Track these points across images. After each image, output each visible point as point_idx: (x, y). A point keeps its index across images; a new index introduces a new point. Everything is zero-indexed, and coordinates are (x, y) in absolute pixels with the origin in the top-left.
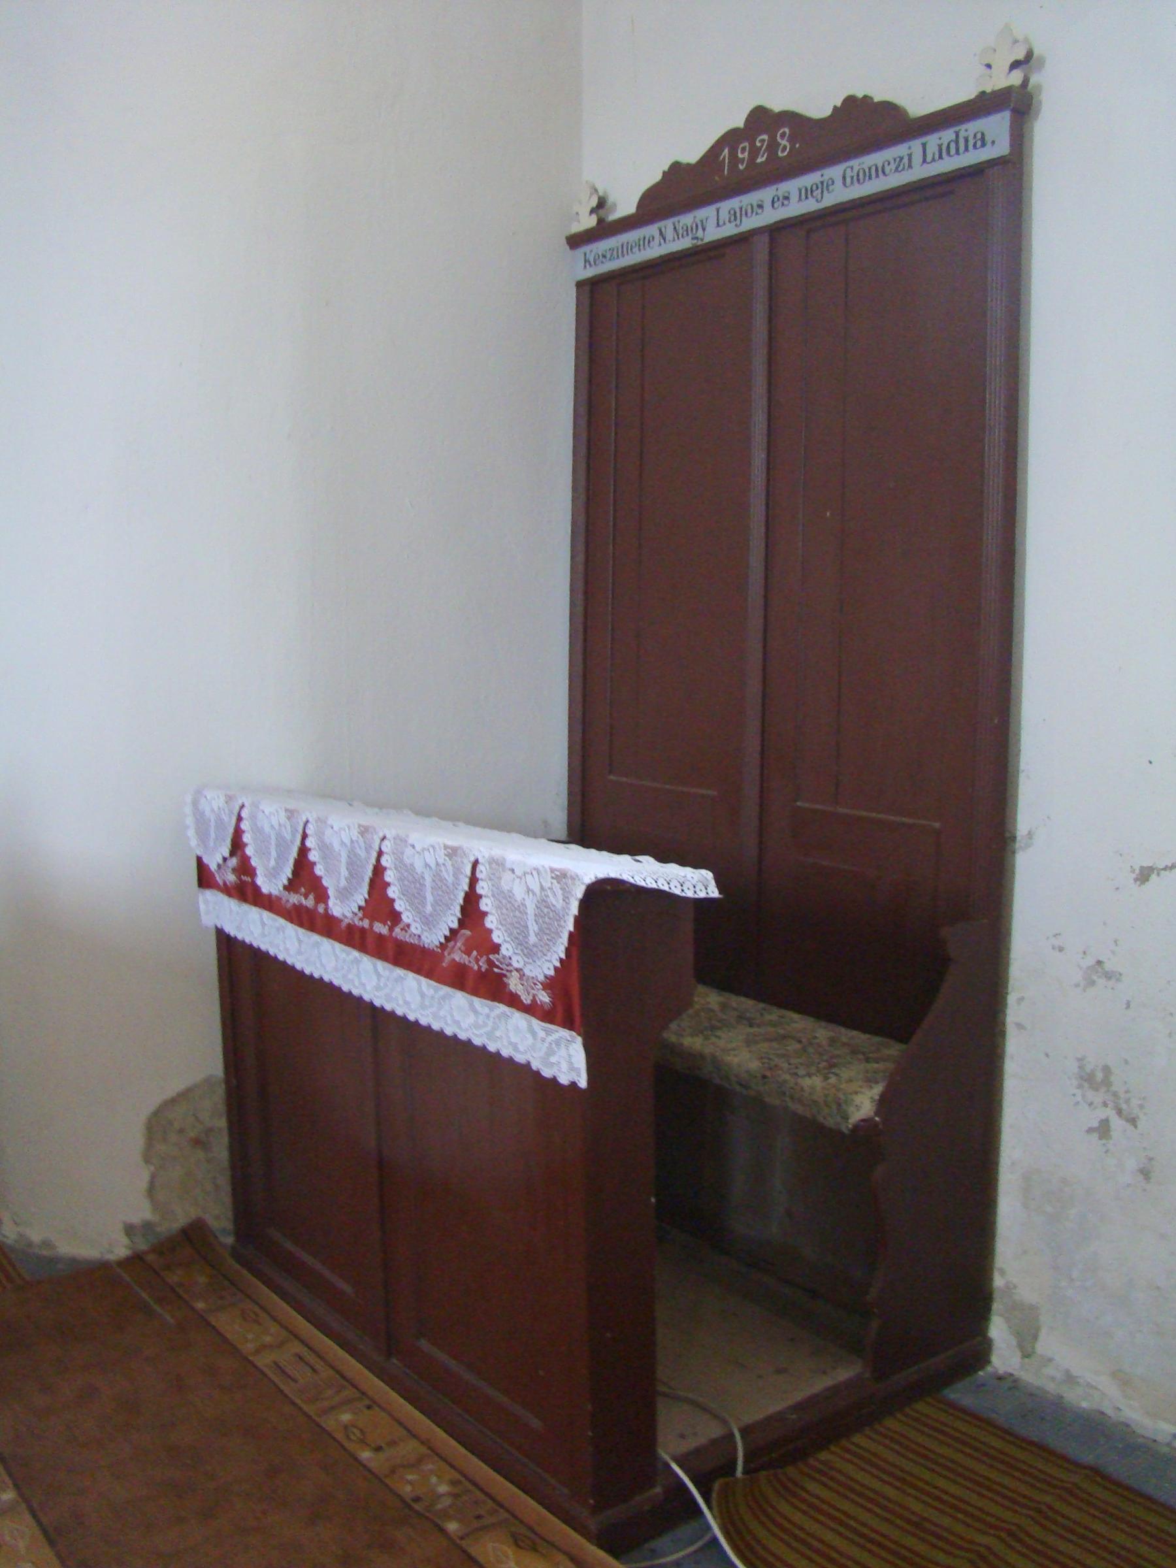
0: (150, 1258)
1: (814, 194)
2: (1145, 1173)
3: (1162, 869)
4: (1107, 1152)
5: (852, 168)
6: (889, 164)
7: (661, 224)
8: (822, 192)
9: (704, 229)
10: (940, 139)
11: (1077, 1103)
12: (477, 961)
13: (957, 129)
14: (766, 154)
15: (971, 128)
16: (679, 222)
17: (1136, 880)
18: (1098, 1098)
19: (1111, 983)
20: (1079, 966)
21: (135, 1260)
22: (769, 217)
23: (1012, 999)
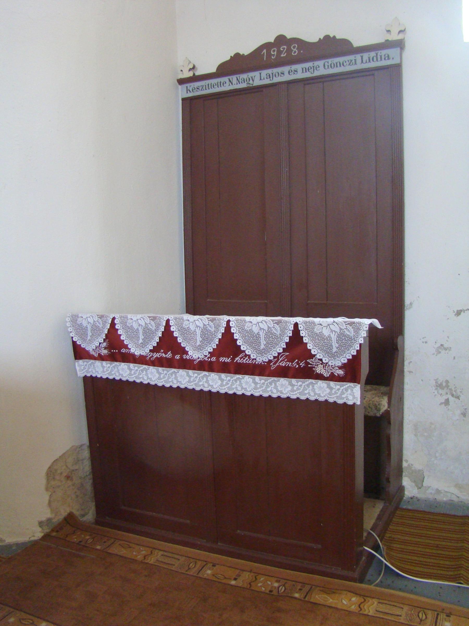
0: (54, 534)
1: (310, 70)
2: (464, 414)
3: (465, 310)
4: (448, 410)
5: (328, 62)
6: (346, 62)
7: (230, 77)
8: (314, 70)
9: (253, 81)
10: (369, 55)
11: (435, 395)
12: (298, 363)
13: (377, 52)
14: (286, 54)
15: (383, 52)
16: (239, 77)
17: (455, 315)
18: (443, 392)
19: (447, 351)
20: (434, 347)
21: (46, 537)
22: (287, 78)
23: (406, 363)
